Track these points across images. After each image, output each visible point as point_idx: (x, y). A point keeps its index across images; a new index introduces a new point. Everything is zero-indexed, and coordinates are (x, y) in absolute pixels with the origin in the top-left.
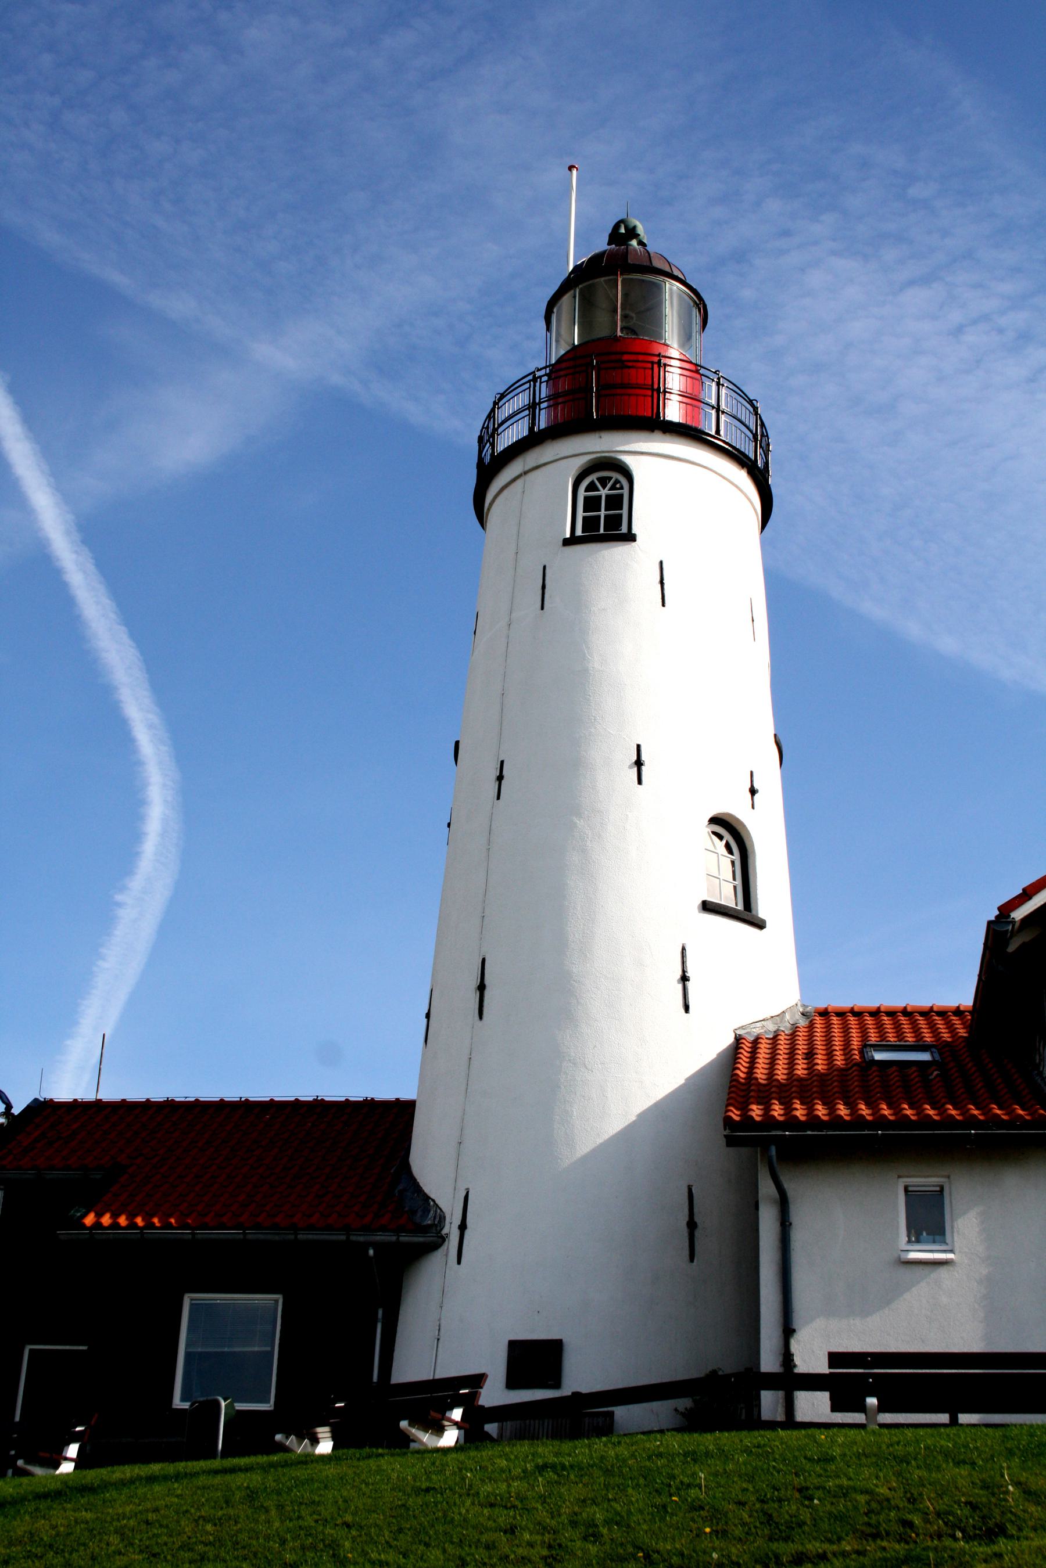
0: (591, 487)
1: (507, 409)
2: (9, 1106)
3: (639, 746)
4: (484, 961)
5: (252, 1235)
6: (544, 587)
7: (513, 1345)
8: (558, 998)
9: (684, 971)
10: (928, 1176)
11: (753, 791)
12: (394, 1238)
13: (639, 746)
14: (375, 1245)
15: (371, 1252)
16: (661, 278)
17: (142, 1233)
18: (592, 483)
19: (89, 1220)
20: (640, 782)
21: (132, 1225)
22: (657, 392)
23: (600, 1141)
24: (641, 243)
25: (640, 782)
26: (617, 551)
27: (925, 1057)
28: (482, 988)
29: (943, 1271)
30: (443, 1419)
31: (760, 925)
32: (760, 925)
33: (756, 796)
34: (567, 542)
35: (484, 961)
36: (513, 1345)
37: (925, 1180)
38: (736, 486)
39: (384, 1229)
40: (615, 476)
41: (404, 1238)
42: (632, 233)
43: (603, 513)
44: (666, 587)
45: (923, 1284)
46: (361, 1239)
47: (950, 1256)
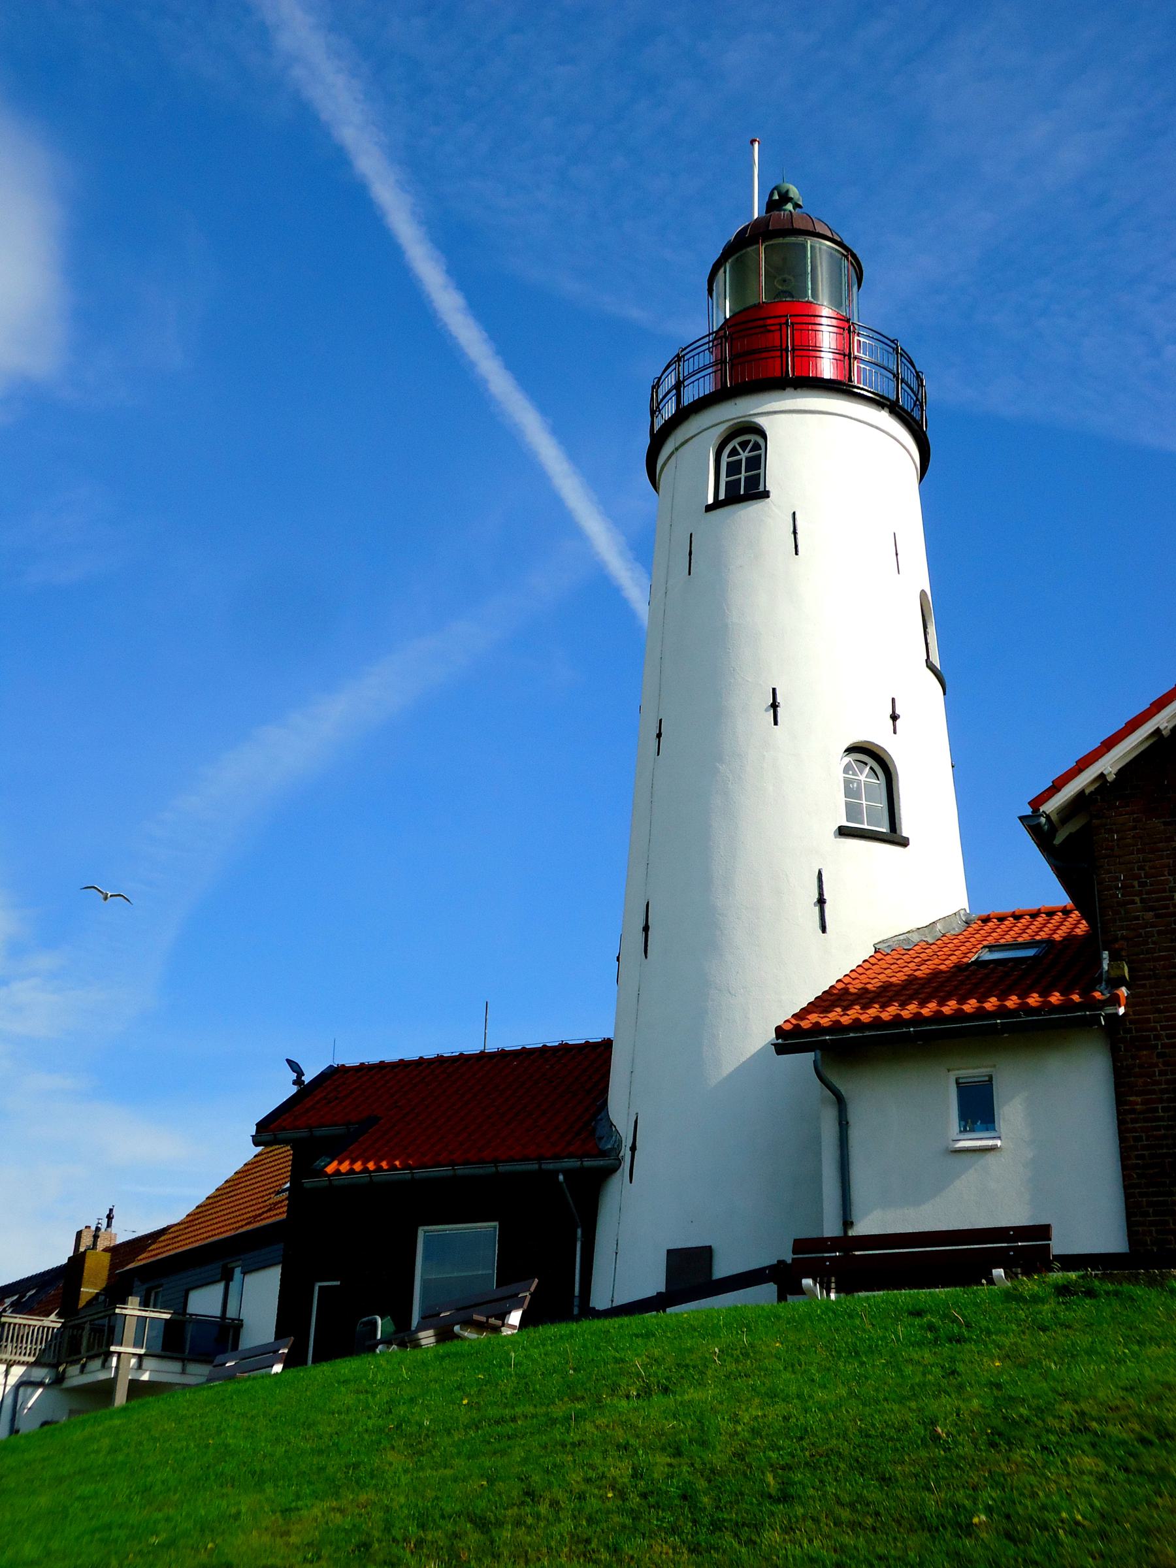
0: (734, 452)
1: (662, 391)
2: (300, 1073)
3: (774, 690)
4: (820, 873)
5: (461, 1170)
6: (795, 532)
7: (669, 1252)
8: (706, 933)
9: (821, 894)
10: (978, 1067)
11: (894, 717)
12: (536, 1167)
13: (774, 690)
14: (566, 1172)
15: (561, 1177)
16: (801, 239)
17: (330, 1180)
18: (734, 449)
19: (330, 1169)
20: (776, 723)
21: (379, 1169)
22: (809, 351)
23: (743, 1059)
24: (797, 206)
25: (776, 723)
26: (754, 508)
27: (1030, 953)
28: (646, 929)
29: (990, 1158)
30: (503, 1325)
31: (904, 843)
32: (904, 843)
33: (898, 722)
34: (709, 508)
35: (820, 873)
36: (669, 1252)
37: (973, 1071)
38: (877, 428)
39: (570, 1156)
40: (753, 438)
41: (588, 1163)
42: (785, 198)
43: (743, 476)
44: (798, 536)
45: (971, 1171)
46: (551, 1166)
47: (999, 1143)
